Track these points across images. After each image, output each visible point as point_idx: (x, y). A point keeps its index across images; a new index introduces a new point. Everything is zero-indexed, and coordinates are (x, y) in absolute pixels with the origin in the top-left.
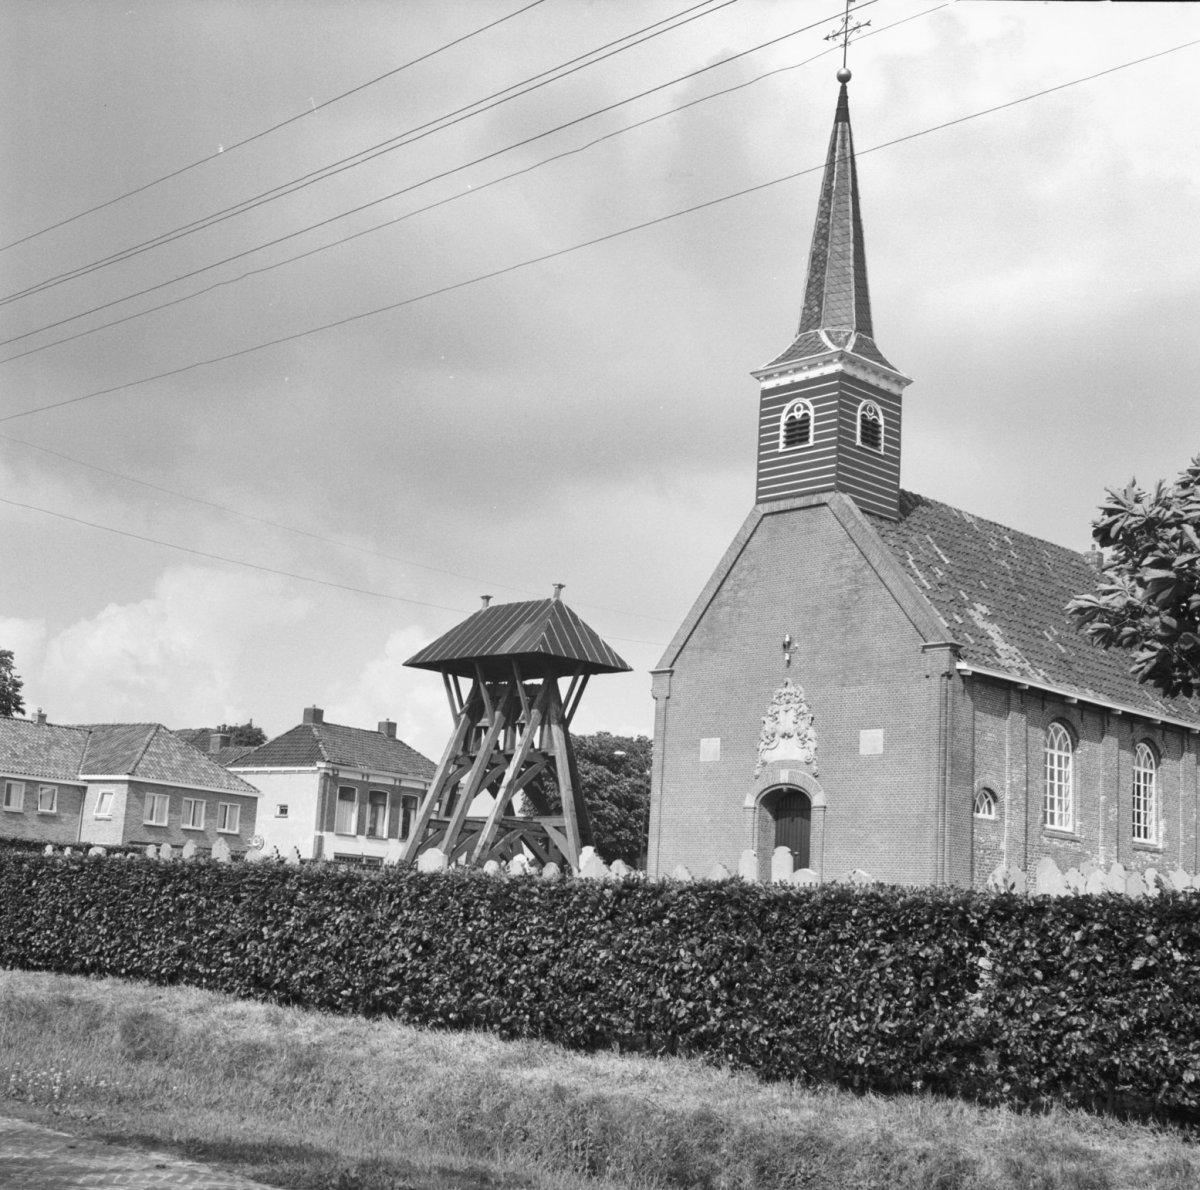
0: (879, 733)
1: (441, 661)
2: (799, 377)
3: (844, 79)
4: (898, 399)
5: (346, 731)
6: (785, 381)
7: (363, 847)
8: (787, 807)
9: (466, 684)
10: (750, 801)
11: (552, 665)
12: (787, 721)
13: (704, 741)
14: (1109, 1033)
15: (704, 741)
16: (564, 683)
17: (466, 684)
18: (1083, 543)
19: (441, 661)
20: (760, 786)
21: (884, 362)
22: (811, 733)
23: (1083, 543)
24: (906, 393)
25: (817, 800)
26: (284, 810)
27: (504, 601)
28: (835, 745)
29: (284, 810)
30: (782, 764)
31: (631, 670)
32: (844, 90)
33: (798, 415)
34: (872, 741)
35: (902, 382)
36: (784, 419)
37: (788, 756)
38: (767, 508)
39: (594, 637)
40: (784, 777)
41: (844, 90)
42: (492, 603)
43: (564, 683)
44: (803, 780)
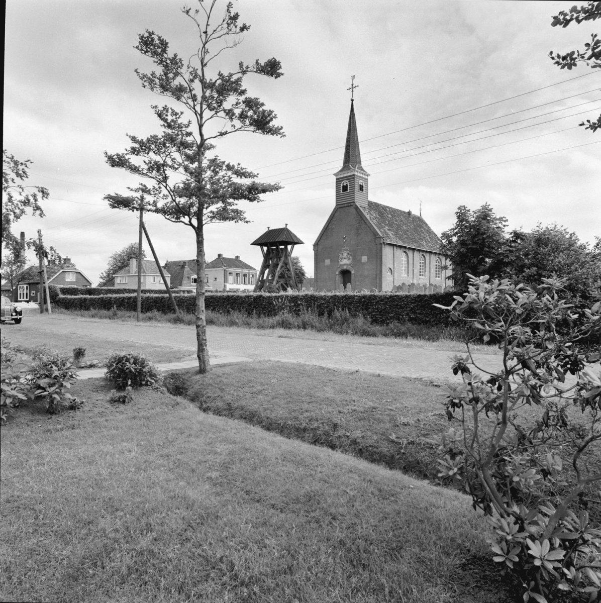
0: (366, 257)
1: (259, 243)
2: (345, 175)
3: (352, 100)
4: (367, 179)
5: (228, 259)
6: (342, 176)
7: (235, 287)
8: (346, 275)
9: (265, 248)
10: (337, 273)
11: (286, 243)
12: (345, 255)
13: (326, 261)
14: (208, 501)
15: (326, 261)
16: (289, 247)
17: (265, 248)
18: (439, 235)
19: (259, 243)
20: (339, 270)
21: (364, 171)
22: (351, 258)
23: (439, 235)
24: (369, 178)
25: (353, 272)
26: (216, 278)
27: (273, 228)
28: (356, 260)
29: (216, 278)
30: (345, 264)
31: (302, 243)
32: (352, 103)
33: (345, 184)
34: (364, 259)
35: (368, 175)
36: (342, 185)
37: (345, 262)
38: (338, 207)
39: (295, 236)
40: (345, 267)
41: (352, 103)
42: (270, 229)
43: (289, 247)
44: (349, 268)
